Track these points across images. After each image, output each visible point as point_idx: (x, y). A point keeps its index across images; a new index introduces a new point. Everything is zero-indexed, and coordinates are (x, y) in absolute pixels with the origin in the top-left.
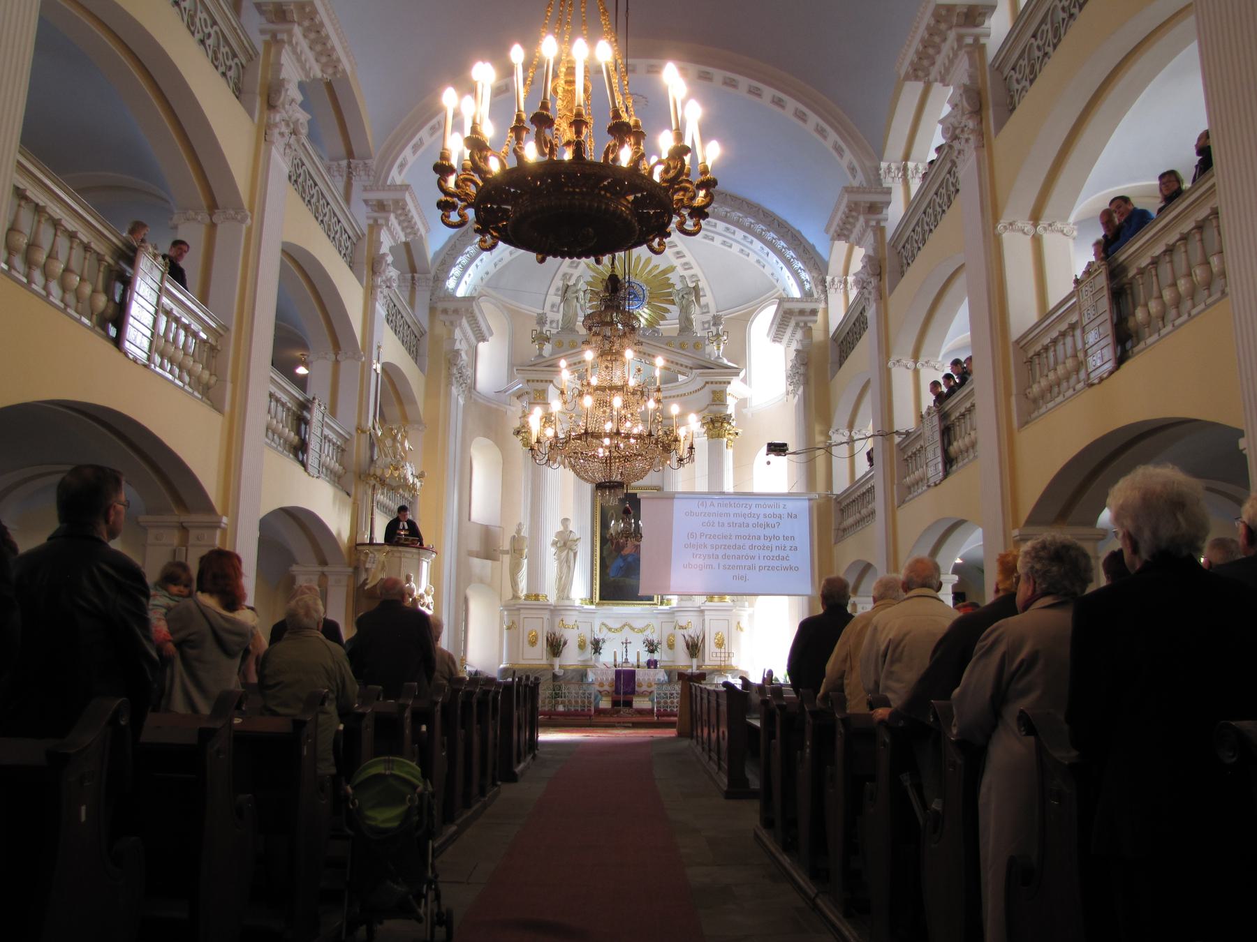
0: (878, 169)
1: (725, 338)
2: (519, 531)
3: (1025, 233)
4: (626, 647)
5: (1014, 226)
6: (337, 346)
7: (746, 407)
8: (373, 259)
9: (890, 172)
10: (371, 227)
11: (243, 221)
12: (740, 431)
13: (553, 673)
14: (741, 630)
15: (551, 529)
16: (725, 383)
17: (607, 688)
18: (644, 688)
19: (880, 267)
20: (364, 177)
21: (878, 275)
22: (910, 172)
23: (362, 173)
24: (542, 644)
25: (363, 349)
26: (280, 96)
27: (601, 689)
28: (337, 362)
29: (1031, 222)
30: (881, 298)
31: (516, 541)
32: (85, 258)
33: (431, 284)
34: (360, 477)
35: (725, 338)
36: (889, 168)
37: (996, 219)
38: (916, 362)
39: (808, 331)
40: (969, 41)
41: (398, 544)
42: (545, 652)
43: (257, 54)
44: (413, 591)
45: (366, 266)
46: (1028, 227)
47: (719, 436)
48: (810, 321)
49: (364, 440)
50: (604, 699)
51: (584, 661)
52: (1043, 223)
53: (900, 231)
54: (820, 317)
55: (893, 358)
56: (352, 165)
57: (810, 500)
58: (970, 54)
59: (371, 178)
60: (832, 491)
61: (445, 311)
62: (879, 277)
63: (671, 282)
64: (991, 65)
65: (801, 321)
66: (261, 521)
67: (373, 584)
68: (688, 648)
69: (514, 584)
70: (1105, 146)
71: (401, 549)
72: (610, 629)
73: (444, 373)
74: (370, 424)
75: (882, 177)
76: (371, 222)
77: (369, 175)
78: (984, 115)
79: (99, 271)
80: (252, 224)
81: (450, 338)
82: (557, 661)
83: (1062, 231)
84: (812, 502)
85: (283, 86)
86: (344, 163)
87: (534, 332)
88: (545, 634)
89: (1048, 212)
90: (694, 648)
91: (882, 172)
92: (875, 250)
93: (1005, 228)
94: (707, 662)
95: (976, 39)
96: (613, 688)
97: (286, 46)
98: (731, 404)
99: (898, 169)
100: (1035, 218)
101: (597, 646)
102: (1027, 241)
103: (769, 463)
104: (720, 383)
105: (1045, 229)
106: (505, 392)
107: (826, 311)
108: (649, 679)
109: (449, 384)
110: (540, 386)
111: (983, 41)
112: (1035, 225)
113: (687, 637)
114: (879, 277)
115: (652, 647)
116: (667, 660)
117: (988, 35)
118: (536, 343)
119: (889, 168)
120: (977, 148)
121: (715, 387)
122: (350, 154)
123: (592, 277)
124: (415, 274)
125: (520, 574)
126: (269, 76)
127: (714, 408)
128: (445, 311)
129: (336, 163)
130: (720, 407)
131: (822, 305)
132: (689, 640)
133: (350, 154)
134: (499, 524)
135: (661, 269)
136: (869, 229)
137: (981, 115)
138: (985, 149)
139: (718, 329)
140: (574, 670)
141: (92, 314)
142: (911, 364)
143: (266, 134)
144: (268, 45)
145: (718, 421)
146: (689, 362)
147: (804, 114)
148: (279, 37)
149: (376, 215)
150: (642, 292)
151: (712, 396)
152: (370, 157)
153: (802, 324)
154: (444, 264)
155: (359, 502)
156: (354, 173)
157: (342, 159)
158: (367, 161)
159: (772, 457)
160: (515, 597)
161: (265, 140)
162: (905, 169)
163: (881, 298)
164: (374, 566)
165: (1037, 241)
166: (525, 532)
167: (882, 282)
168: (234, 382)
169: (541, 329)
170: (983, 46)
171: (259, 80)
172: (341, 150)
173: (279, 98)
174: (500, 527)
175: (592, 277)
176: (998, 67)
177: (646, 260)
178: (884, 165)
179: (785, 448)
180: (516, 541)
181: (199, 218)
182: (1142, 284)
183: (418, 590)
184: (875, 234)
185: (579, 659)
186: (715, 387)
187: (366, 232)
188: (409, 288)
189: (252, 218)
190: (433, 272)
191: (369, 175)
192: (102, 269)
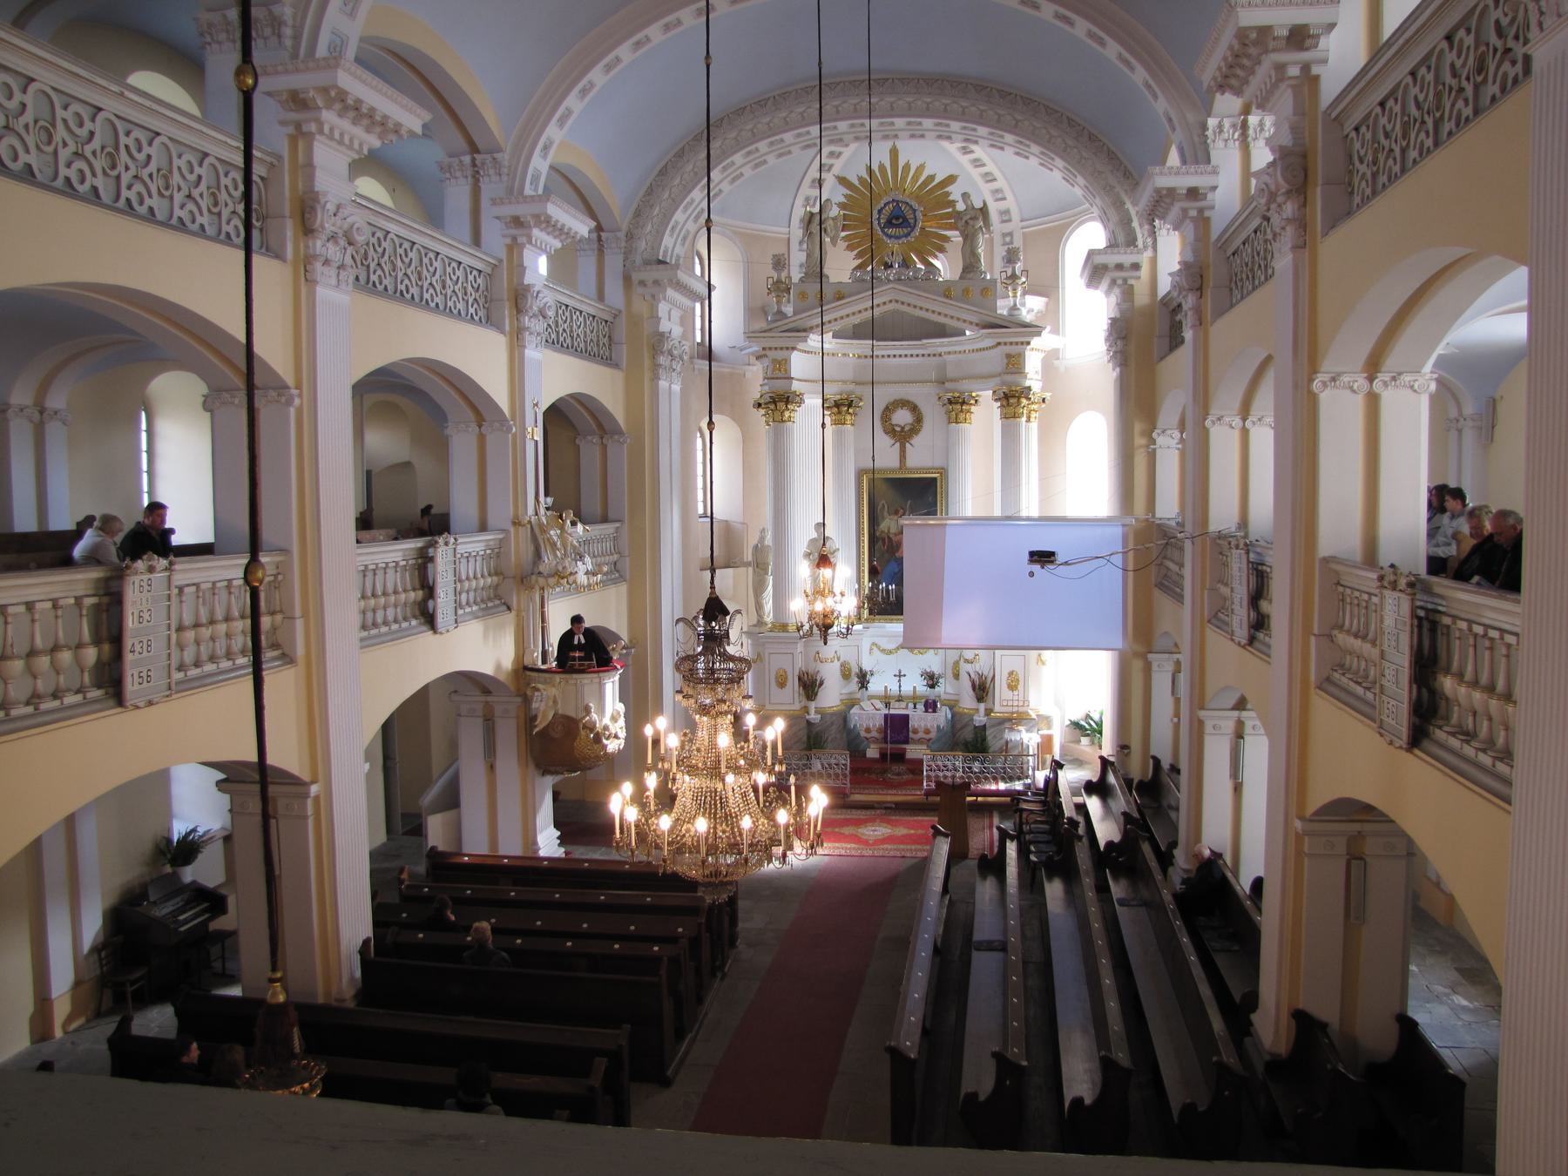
0: (1204, 127)
1: (1024, 279)
2: (762, 539)
3: (1354, 391)
4: (900, 681)
5: (1338, 383)
6: (480, 420)
7: (1058, 359)
8: (516, 290)
9: (1221, 131)
10: (510, 248)
11: (289, 402)
12: (1048, 395)
13: (807, 721)
14: (1043, 663)
15: (802, 535)
16: (1022, 343)
17: (874, 734)
18: (921, 735)
19: (1201, 276)
20: (495, 178)
21: (1197, 290)
22: (1251, 132)
23: (491, 172)
24: (793, 684)
25: (513, 418)
26: (316, 215)
27: (868, 736)
28: (482, 439)
29: (1366, 375)
30: (1201, 324)
31: (759, 550)
32: (57, 617)
33: (623, 244)
34: (522, 581)
35: (1024, 279)
36: (1220, 126)
37: (1314, 371)
38: (1244, 420)
39: (1128, 293)
40: (1294, 71)
41: (573, 671)
42: (796, 695)
43: (279, 158)
44: (595, 723)
45: (507, 304)
46: (1361, 382)
47: (1015, 416)
48: (1132, 278)
49: (524, 533)
50: (872, 746)
51: (850, 693)
52: (1383, 376)
53: (1231, 231)
54: (1145, 271)
55: (1214, 412)
56: (477, 162)
57: (1124, 525)
58: (1297, 90)
59: (505, 178)
60: (1154, 516)
61: (642, 283)
62: (1199, 293)
63: (951, 198)
64: (1326, 112)
65: (1119, 278)
66: (366, 751)
67: (542, 726)
68: (974, 689)
69: (759, 607)
70: (1152, 1044)
71: (575, 676)
72: (883, 651)
73: (647, 362)
74: (531, 511)
75: (1209, 141)
76: (508, 241)
77: (500, 175)
78: (1308, 193)
79: (81, 616)
80: (302, 404)
81: (653, 317)
82: (812, 705)
83: (1412, 387)
84: (1126, 528)
85: (319, 202)
86: (467, 159)
87: (770, 281)
88: (797, 673)
89: (1391, 362)
90: (982, 690)
91: (1209, 133)
92: (1195, 252)
93: (1324, 384)
94: (997, 708)
95: (1306, 68)
96: (882, 735)
97: (318, 137)
98: (1033, 363)
99: (1234, 126)
100: (1373, 367)
101: (863, 680)
102: (1357, 403)
103: (1032, 574)
104: (1017, 343)
105: (1385, 384)
106: (741, 350)
107: (1154, 262)
108: (926, 725)
109: (655, 378)
110: (780, 355)
111: (1315, 70)
112: (1371, 379)
113: (973, 676)
114: (1199, 293)
115: (932, 680)
116: (951, 692)
117: (1325, 61)
118: (773, 294)
119: (1220, 126)
120: (1295, 248)
121: (1008, 349)
122: (474, 149)
123: (846, 196)
124: (602, 234)
125: (765, 595)
126: (300, 186)
127: (1009, 378)
128: (642, 283)
129: (457, 160)
130: (1017, 376)
131: (1148, 254)
132: (977, 680)
133: (474, 149)
134: (741, 520)
135: (937, 181)
136: (1188, 221)
137: (1305, 193)
138: (1307, 249)
139: (1014, 269)
140: (832, 714)
141: (82, 671)
142: (1237, 422)
143: (306, 271)
144: (293, 140)
145: (1014, 396)
146: (975, 319)
147: (1102, 39)
148: (305, 128)
149: (513, 232)
150: (912, 216)
151: (1005, 361)
152: (500, 150)
153: (1120, 282)
154: (639, 215)
155: (523, 614)
156: (482, 173)
157: (463, 154)
158: (495, 155)
159: (1036, 568)
160: (760, 623)
161: (306, 280)
162: (1244, 125)
163: (1201, 324)
164: (543, 704)
165: (1373, 402)
166: (769, 541)
167: (1202, 300)
168: (305, 615)
169: (779, 276)
170: (1317, 78)
171: (287, 193)
172: (461, 144)
173: (315, 220)
174: (743, 523)
175: (846, 196)
176: (1335, 119)
177: (917, 168)
178: (1212, 122)
179: (1052, 558)
180: (759, 550)
181: (237, 401)
182: (1459, 638)
183: (601, 721)
184: (1196, 228)
185: (844, 691)
186: (1008, 349)
187: (504, 256)
188: (596, 252)
189: (300, 396)
190: (624, 227)
191: (500, 175)
192: (84, 612)
